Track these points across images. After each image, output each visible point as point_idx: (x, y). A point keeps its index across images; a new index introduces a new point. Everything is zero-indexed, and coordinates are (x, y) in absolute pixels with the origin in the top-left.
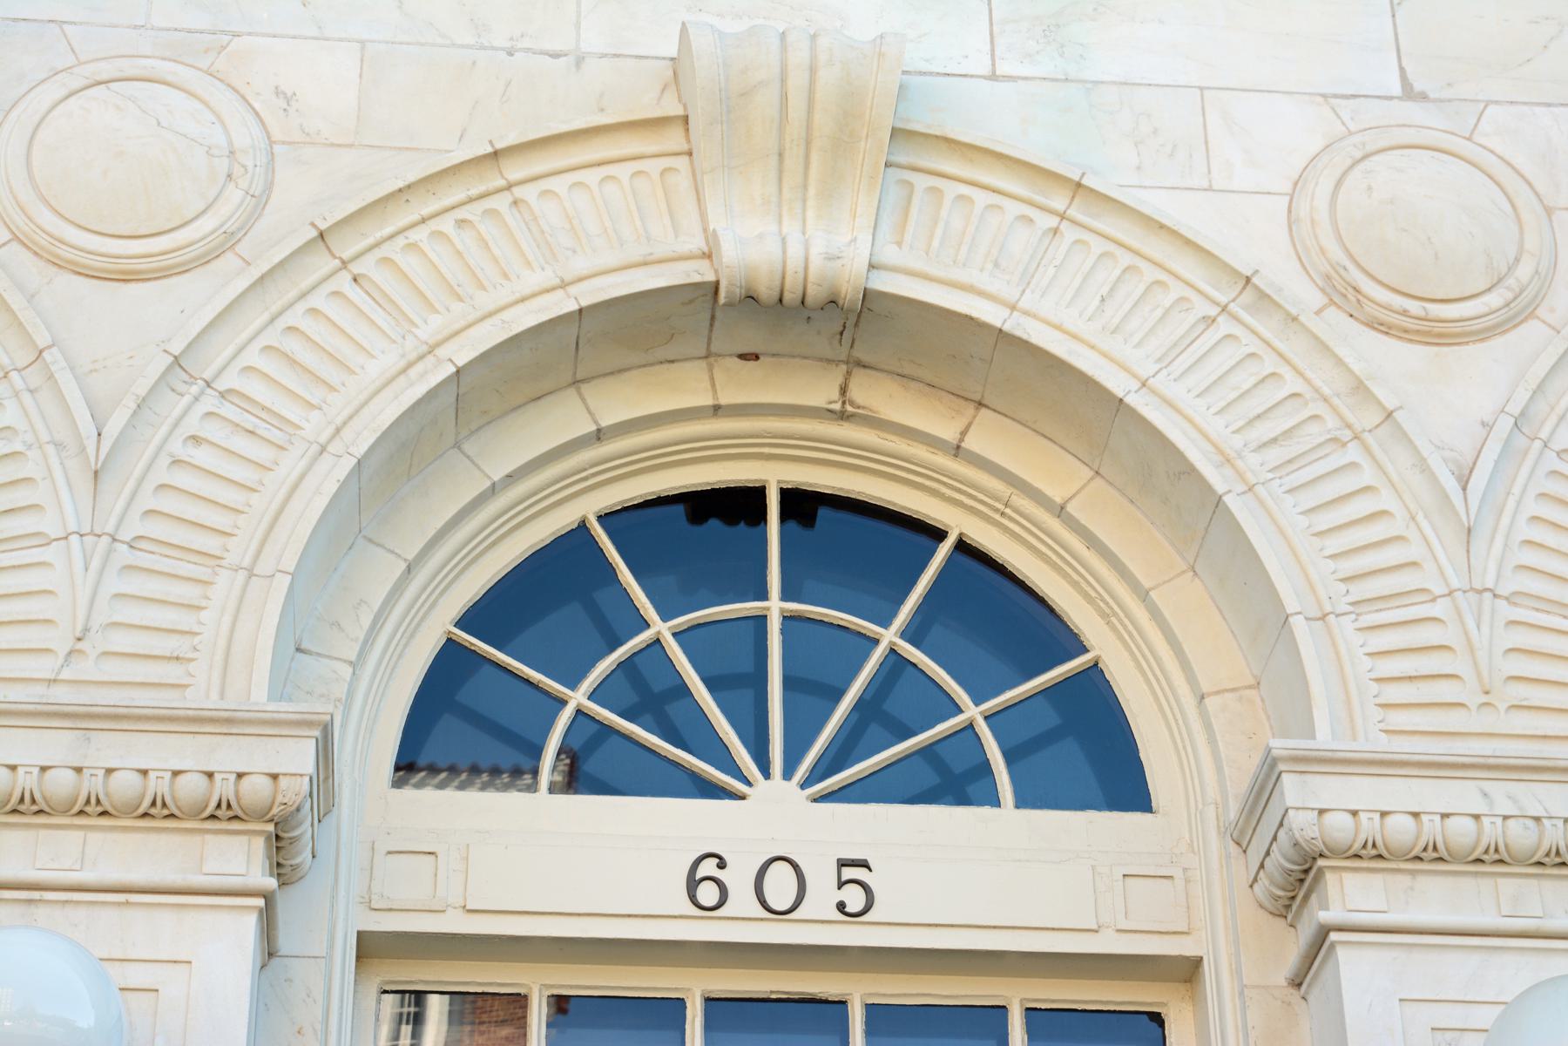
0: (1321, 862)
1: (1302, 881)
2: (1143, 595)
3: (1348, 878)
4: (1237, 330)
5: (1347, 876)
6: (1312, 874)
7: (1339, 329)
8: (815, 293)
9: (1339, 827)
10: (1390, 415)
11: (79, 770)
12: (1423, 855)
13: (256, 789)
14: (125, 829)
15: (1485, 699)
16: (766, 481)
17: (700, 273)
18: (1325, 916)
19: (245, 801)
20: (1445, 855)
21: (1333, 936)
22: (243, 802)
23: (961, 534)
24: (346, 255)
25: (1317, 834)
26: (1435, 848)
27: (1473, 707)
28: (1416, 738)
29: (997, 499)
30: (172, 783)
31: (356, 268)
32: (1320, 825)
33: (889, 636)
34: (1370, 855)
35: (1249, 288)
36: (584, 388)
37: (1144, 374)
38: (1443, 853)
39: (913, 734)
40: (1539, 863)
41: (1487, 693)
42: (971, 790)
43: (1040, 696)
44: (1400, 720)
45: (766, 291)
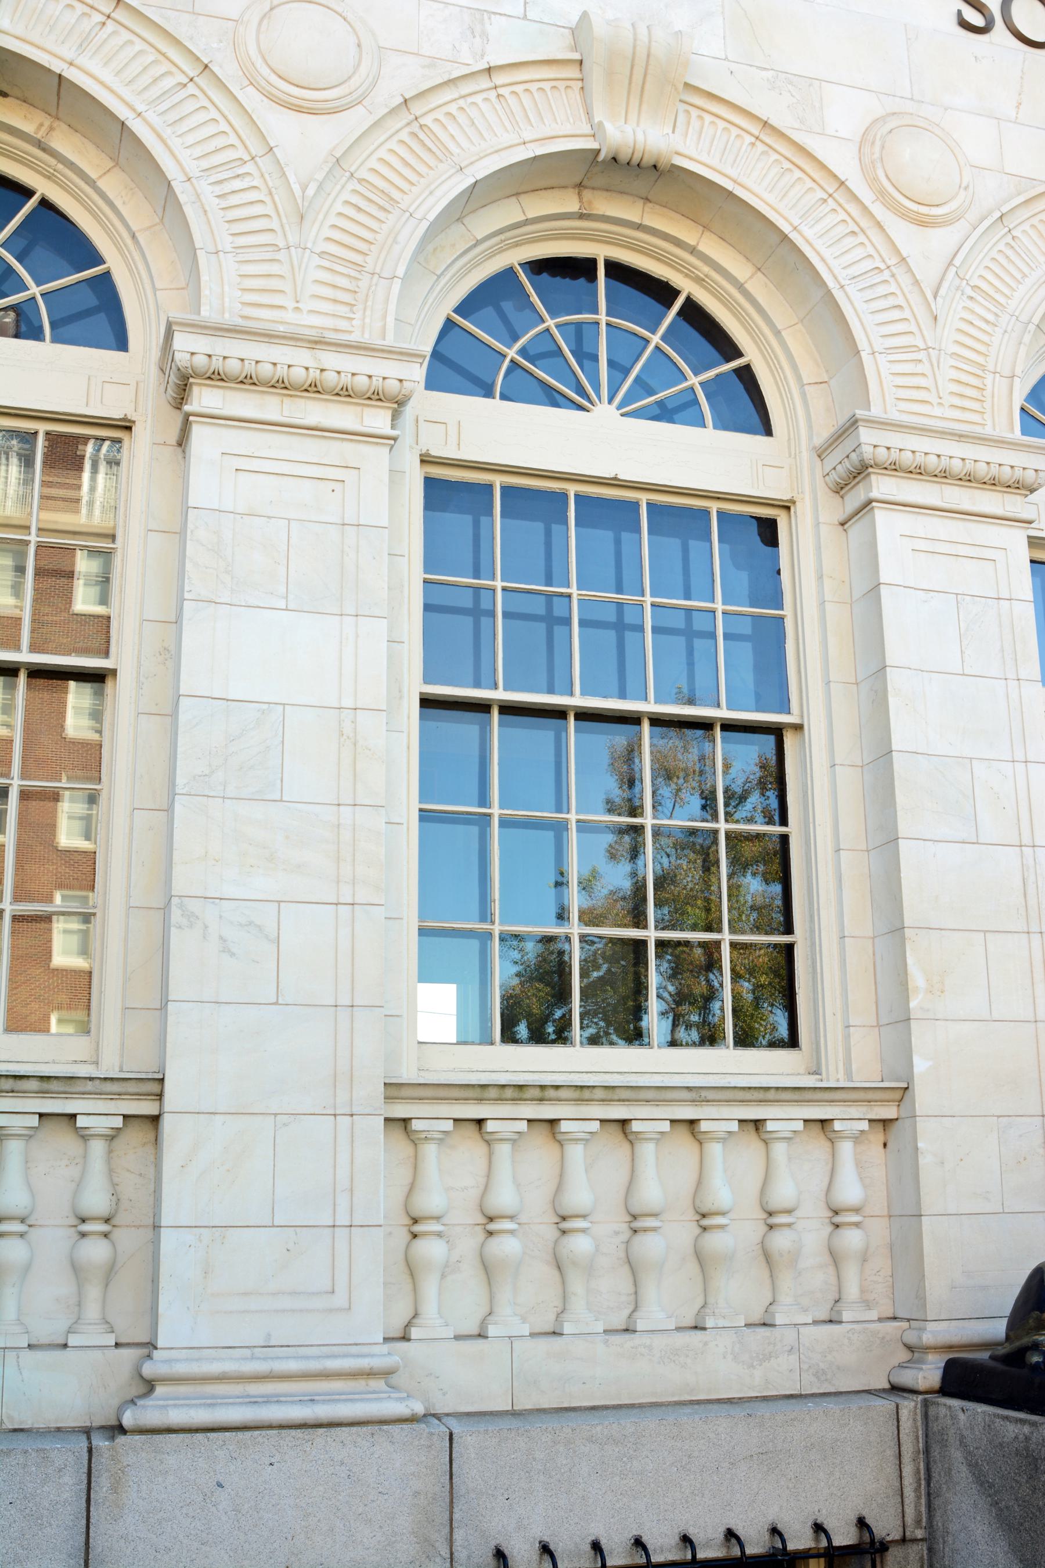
0: (191, 380)
1: (855, 477)
2: (777, 333)
3: (205, 390)
4: (197, 92)
5: (204, 388)
6: (862, 476)
7: (250, 98)
8: (648, 161)
9: (882, 454)
10: (271, 149)
11: (939, 456)
12: (309, 389)
13: (392, 386)
14: (231, 388)
15: (296, 305)
16: (598, 255)
17: (591, 145)
18: (875, 494)
19: (227, 370)
20: (320, 389)
21: (191, 418)
22: (355, 389)
23: (689, 293)
24: (418, 114)
25: (189, 365)
26: (251, 378)
27: (935, 404)
28: (922, 417)
29: (49, 166)
30: (320, 375)
31: (422, 121)
32: (191, 360)
33: (656, 339)
34: (217, 377)
35: (842, 187)
36: (522, 197)
37: (796, 224)
38: (287, 384)
39: (7, 296)
40: (337, 394)
41: (297, 302)
42: (675, 417)
43: (84, 283)
44: (903, 406)
45: (623, 157)
